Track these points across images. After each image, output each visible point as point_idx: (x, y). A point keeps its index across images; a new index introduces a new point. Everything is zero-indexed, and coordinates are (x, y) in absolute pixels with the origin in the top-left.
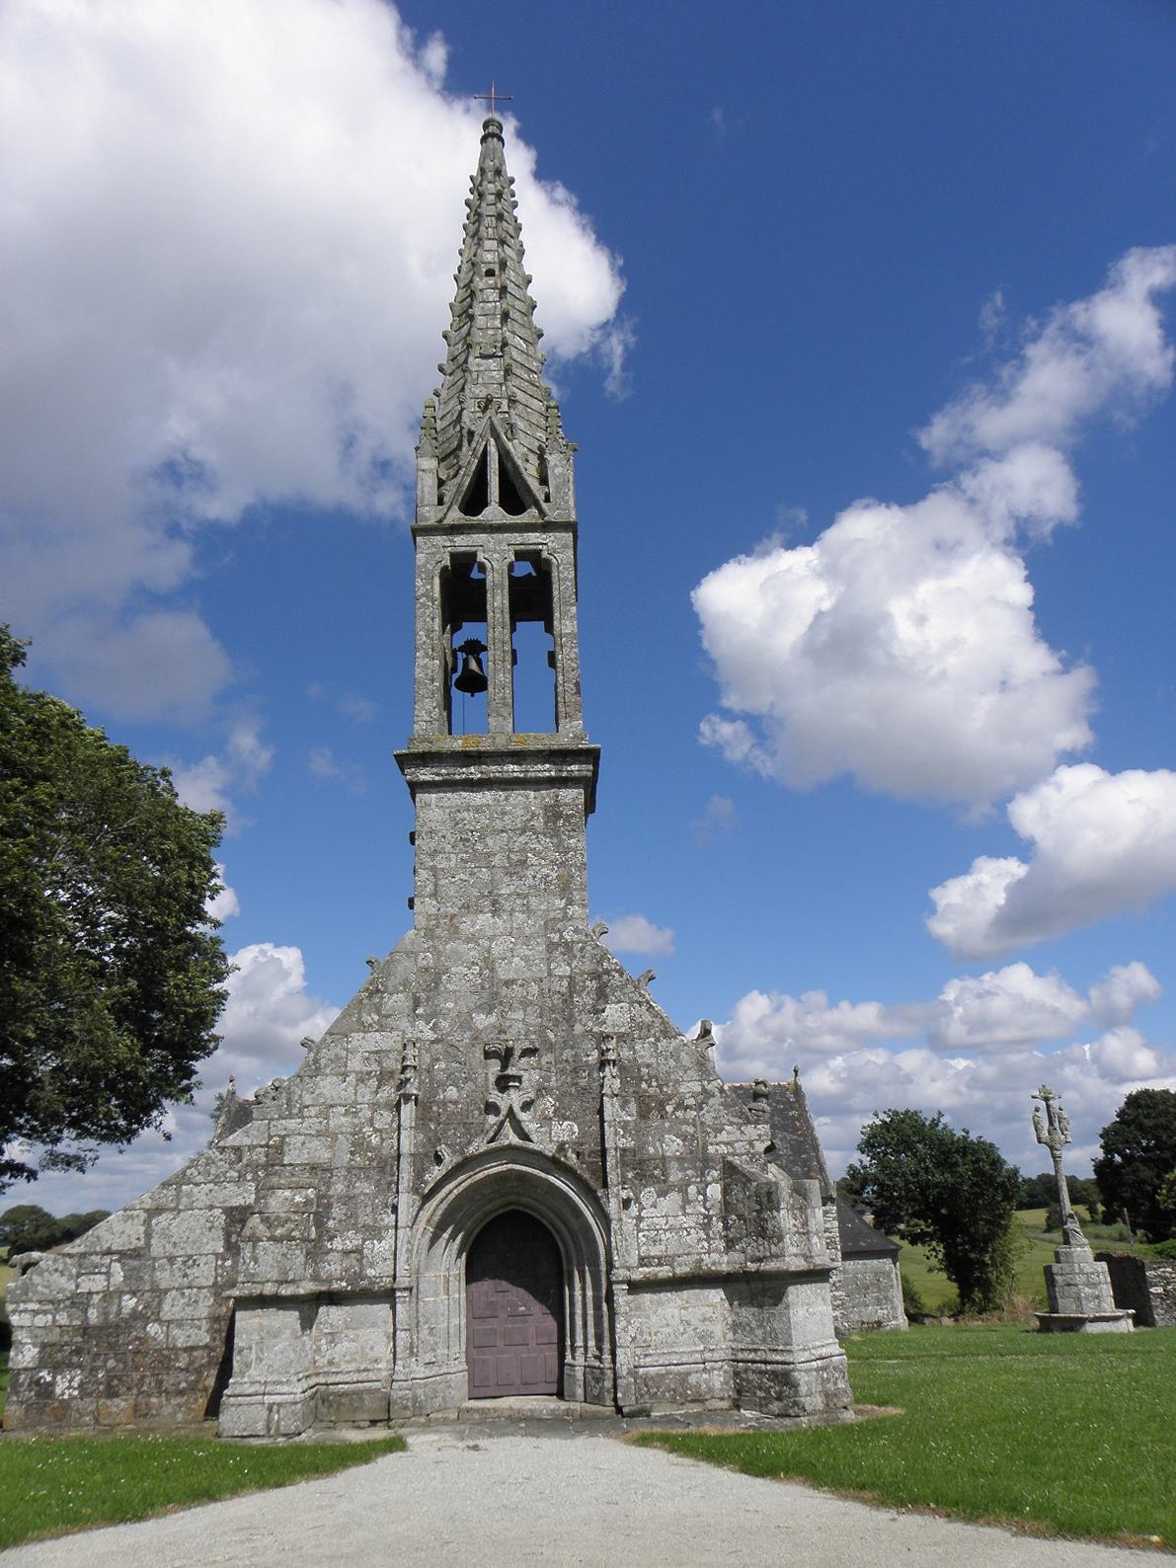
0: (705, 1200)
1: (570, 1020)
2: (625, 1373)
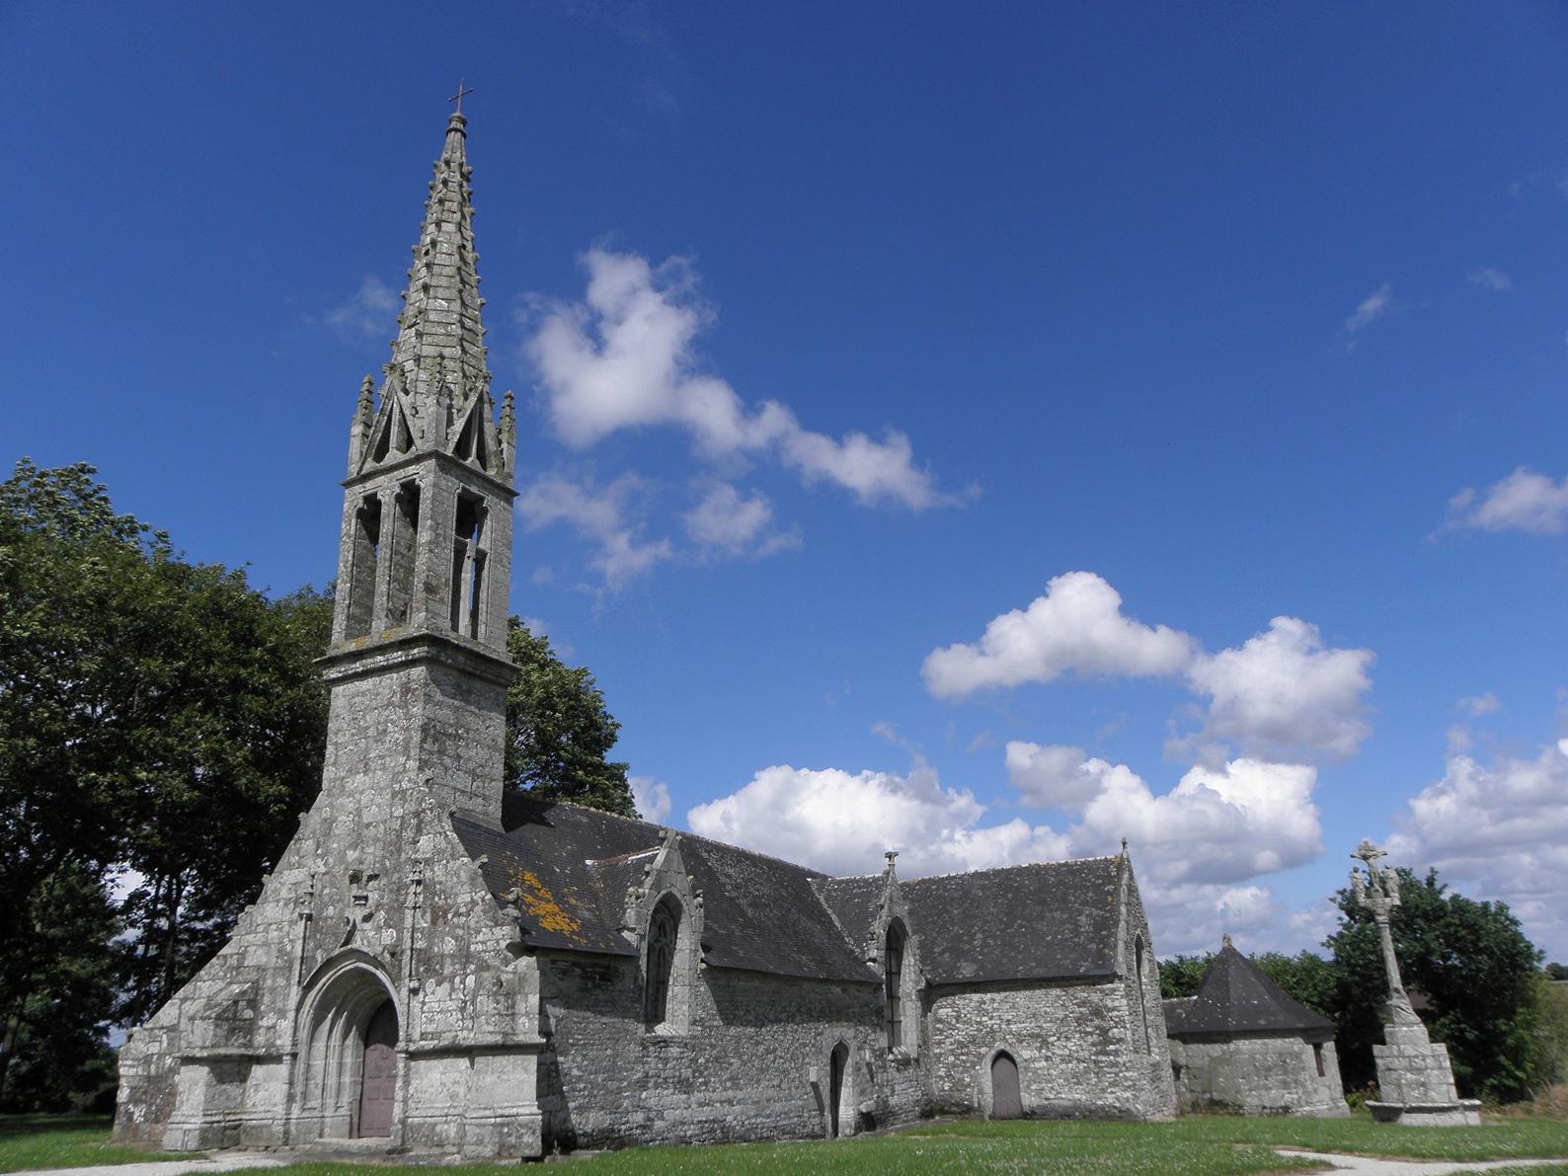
0: (464, 988)
1: (399, 851)
2: (396, 1121)
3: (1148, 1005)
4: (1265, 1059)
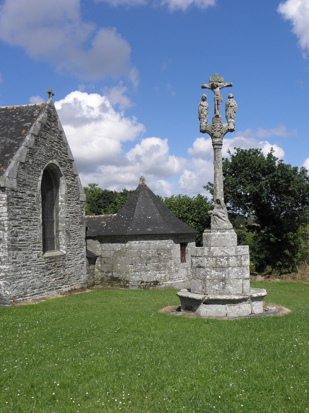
3: (62, 216)
4: (148, 253)
